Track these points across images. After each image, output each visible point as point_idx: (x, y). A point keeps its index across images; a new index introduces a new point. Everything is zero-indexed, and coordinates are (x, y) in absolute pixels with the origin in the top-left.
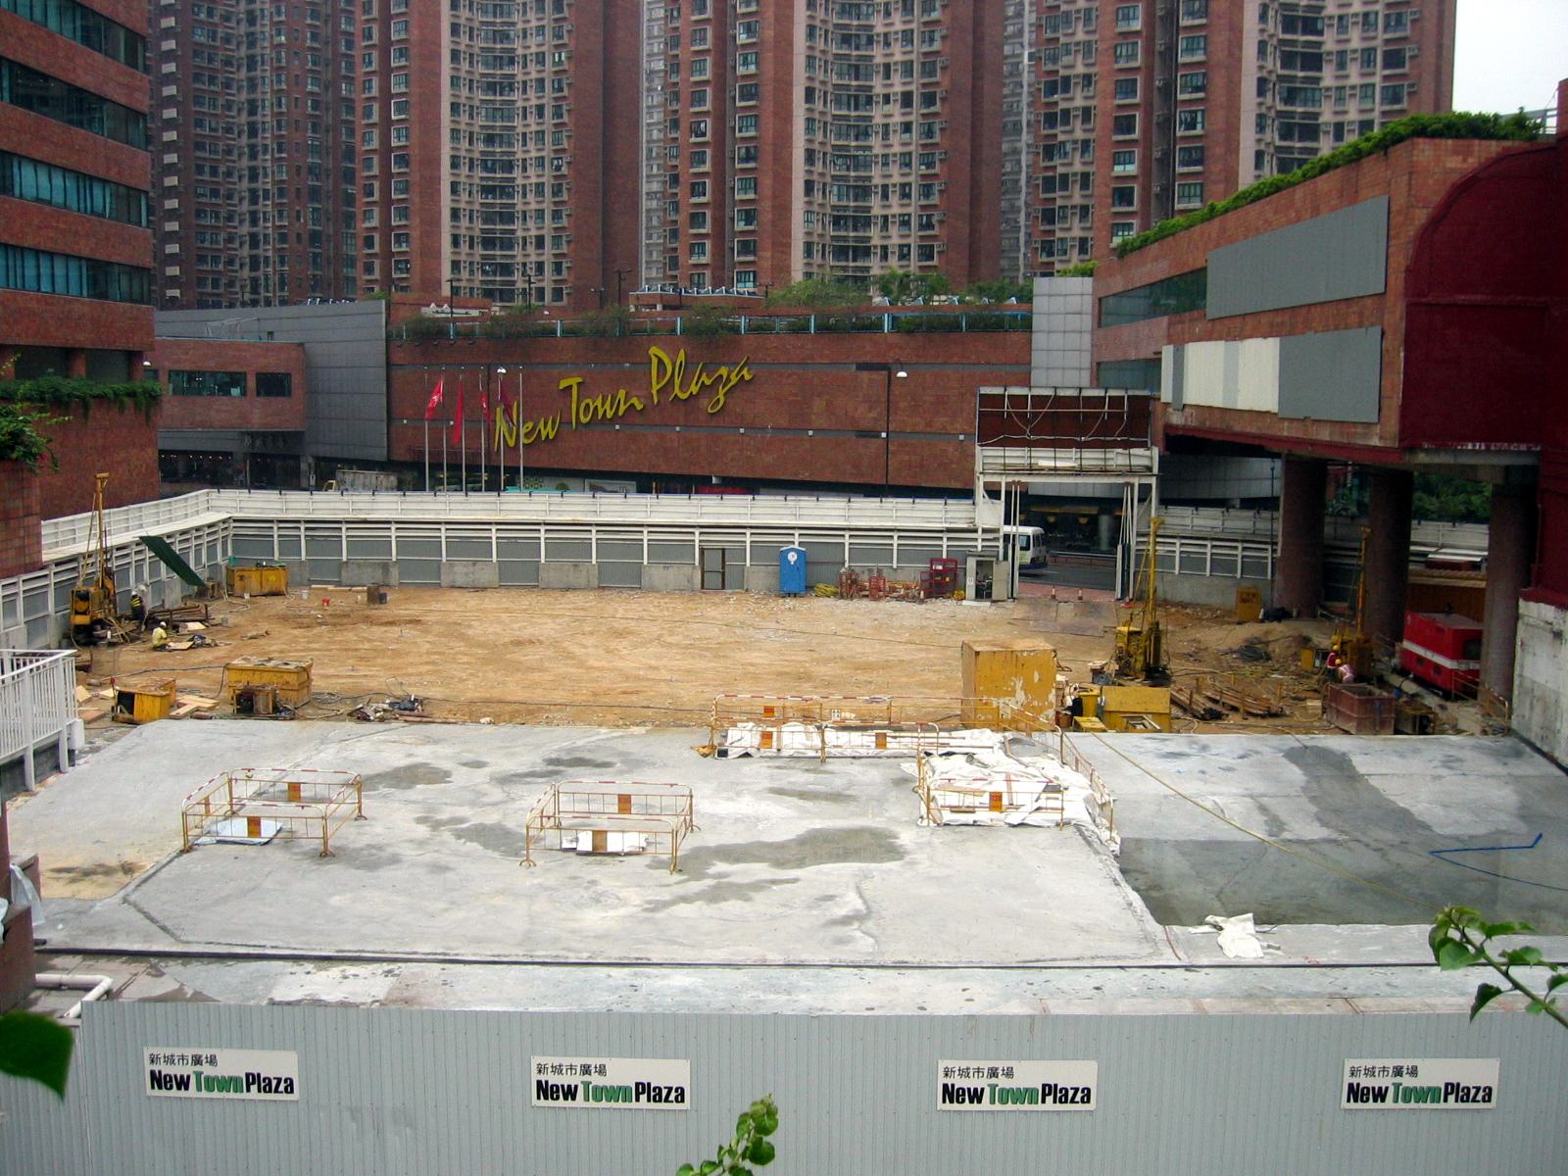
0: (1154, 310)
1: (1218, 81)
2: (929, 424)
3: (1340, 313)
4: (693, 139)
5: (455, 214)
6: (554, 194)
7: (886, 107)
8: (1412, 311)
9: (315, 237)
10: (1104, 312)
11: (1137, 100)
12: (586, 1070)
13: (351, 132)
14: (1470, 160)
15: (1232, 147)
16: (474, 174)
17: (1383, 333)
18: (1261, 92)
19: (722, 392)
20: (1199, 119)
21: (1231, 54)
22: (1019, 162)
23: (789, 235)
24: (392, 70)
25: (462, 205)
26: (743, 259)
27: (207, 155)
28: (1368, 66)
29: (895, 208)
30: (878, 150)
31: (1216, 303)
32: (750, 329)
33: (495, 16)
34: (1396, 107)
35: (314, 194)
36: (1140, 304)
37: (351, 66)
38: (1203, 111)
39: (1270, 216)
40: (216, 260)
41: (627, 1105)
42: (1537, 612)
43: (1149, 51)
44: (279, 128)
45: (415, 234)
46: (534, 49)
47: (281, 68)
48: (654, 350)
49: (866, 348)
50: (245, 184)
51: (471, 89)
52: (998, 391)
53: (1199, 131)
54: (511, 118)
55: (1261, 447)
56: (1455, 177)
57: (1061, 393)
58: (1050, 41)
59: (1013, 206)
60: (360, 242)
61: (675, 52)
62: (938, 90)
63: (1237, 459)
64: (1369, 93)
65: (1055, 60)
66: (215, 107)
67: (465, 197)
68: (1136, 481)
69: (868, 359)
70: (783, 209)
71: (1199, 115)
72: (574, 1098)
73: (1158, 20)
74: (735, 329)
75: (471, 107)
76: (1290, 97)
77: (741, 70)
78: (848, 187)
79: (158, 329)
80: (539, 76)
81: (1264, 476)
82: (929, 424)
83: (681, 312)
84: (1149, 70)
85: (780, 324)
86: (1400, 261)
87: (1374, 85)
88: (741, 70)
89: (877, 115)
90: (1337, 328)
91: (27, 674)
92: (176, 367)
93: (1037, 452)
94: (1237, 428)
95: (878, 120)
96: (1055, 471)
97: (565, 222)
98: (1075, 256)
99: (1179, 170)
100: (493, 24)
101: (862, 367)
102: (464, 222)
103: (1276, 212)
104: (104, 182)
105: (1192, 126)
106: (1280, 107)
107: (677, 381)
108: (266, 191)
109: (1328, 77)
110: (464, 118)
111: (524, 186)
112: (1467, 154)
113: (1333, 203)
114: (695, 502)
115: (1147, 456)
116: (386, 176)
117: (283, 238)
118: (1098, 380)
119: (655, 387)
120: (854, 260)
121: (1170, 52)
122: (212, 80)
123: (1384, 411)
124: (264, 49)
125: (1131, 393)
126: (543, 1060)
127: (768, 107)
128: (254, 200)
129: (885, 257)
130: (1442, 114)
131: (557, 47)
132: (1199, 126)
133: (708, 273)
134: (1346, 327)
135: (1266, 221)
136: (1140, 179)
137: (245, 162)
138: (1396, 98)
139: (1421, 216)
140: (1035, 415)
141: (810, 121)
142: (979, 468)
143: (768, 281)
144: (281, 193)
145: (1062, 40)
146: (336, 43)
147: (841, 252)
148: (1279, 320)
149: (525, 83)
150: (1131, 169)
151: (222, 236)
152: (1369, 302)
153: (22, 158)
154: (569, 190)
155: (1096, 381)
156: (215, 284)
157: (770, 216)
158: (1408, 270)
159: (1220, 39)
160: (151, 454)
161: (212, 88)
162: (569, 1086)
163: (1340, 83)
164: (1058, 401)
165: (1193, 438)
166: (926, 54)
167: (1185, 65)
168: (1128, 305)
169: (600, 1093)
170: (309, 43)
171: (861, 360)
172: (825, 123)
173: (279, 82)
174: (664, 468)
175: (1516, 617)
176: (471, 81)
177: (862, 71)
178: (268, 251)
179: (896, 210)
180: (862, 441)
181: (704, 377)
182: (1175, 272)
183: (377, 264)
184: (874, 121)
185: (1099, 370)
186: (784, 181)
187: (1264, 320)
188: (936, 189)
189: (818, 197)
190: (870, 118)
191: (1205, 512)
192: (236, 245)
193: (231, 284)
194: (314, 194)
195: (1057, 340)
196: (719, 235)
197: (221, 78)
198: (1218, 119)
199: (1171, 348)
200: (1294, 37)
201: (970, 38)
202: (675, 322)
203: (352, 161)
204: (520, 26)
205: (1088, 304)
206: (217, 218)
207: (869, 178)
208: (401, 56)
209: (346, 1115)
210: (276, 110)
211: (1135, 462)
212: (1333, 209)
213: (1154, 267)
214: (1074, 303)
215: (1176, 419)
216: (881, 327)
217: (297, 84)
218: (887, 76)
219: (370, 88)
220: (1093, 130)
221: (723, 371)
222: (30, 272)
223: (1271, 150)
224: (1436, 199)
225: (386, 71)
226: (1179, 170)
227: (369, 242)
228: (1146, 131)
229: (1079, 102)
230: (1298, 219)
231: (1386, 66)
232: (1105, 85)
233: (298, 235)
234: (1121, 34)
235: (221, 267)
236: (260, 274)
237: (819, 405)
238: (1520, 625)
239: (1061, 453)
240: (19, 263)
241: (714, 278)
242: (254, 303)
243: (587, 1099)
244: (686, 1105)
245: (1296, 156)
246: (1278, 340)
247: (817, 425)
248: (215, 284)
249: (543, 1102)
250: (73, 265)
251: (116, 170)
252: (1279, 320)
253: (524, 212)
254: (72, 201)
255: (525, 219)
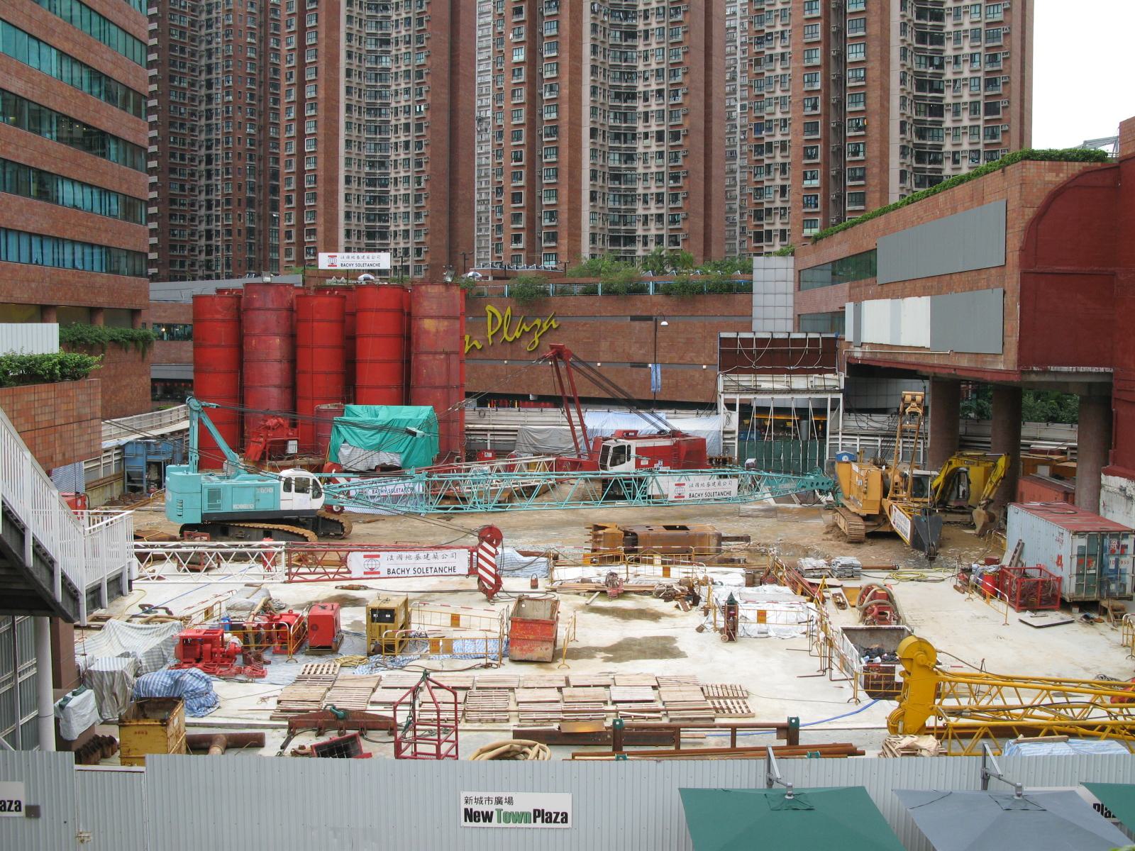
0: (835, 278)
1: (874, 123)
2: (681, 358)
3: (973, 279)
4: (514, 164)
5: (348, 215)
6: (416, 201)
7: (646, 141)
8: (1024, 276)
9: (250, 232)
10: (801, 282)
11: (818, 136)
12: (499, 801)
13: (277, 161)
14: (1061, 175)
15: (885, 168)
16: (361, 188)
17: (1004, 293)
18: (903, 131)
19: (536, 337)
20: (861, 149)
21: (882, 106)
22: (735, 178)
23: (580, 229)
24: (305, 118)
25: (353, 210)
26: (548, 245)
27: (178, 177)
28: (975, 113)
29: (653, 209)
30: (641, 170)
31: (886, 270)
32: (555, 293)
33: (376, 81)
34: (994, 141)
35: (250, 202)
36: (827, 274)
37: (277, 115)
38: (864, 144)
39: (921, 213)
40: (182, 248)
41: (528, 825)
42: (1113, 482)
43: (826, 103)
44: (227, 158)
45: (320, 229)
46: (403, 103)
47: (229, 117)
48: (489, 308)
49: (639, 305)
50: (203, 197)
51: (359, 131)
52: (733, 335)
53: (861, 157)
54: (386, 150)
55: (915, 371)
56: (1051, 187)
57: (776, 336)
58: (757, 96)
59: (731, 208)
60: (282, 235)
61: (499, 105)
62: (681, 130)
63: (894, 380)
64: (976, 132)
65: (761, 109)
66: (184, 144)
67: (354, 203)
68: (829, 396)
69: (639, 313)
70: (575, 211)
71: (861, 146)
72: (490, 821)
73: (831, 83)
74: (545, 292)
75: (360, 143)
76: (921, 134)
77: (546, 117)
78: (620, 195)
79: (152, 296)
80: (407, 139)
81: (914, 394)
82: (681, 358)
83: (508, 281)
84: (827, 115)
85: (577, 289)
86: (1016, 243)
87: (979, 126)
88: (546, 117)
89: (640, 146)
90: (971, 289)
91: (105, 527)
92: (159, 321)
93: (760, 378)
94: (901, 359)
95: (640, 150)
96: (774, 391)
97: (422, 221)
98: (777, 241)
99: (849, 183)
100: (375, 86)
101: (634, 318)
102: (354, 221)
103: (925, 212)
104: (117, 194)
105: (856, 153)
106: (916, 141)
107: (505, 329)
108: (218, 201)
109: (948, 120)
110: (355, 150)
111: (396, 196)
112: (1058, 172)
113: (966, 205)
114: (523, 413)
115: (836, 380)
116: (301, 189)
117: (229, 232)
118: (799, 326)
119: (490, 333)
120: (625, 245)
121: (841, 105)
122: (182, 126)
123: (1006, 346)
124: (218, 104)
125: (823, 336)
126: (469, 794)
127: (565, 142)
128: (209, 207)
129: (645, 244)
130: (1026, 148)
131: (418, 101)
132: (861, 154)
133: (523, 254)
134: (978, 289)
135: (918, 217)
136: (822, 190)
137: (203, 182)
138: (994, 136)
139: (1030, 213)
140: (759, 352)
141: (594, 151)
142: (721, 388)
143: (566, 260)
144: (228, 202)
145: (766, 96)
146: (266, 101)
147: (615, 240)
148: (929, 284)
149: (396, 126)
150: (816, 183)
151: (187, 232)
152: (993, 271)
153: (63, 178)
154: (426, 198)
155: (798, 327)
156: (182, 264)
157: (566, 216)
158: (1021, 250)
159: (874, 95)
160: (146, 381)
161: (182, 131)
162: (487, 813)
163: (957, 125)
164: (774, 341)
165: (868, 365)
166: (672, 105)
167: (851, 112)
168: (818, 275)
169: (509, 817)
170: (248, 101)
171: (634, 314)
172: (604, 152)
173: (228, 127)
174: (496, 390)
175: (1100, 486)
176: (360, 125)
177: (629, 117)
178: (218, 241)
179: (654, 211)
180: (635, 370)
181: (524, 326)
182: (854, 252)
183: (294, 249)
184: (638, 151)
185: (799, 320)
186: (575, 191)
187: (919, 284)
188: (680, 197)
189: (599, 203)
190: (635, 149)
191: (876, 417)
192: (197, 238)
193: (193, 264)
194: (250, 202)
195: (770, 299)
196: (531, 228)
197: (188, 125)
198: (874, 149)
199: (852, 304)
200: (924, 94)
201: (702, 94)
202: (504, 289)
203: (278, 180)
204: (394, 87)
205: (791, 274)
206: (184, 219)
207: (635, 189)
208: (312, 109)
209: (331, 833)
210: (225, 161)
211: (828, 383)
212: (966, 209)
213: (839, 248)
214: (781, 274)
215: (858, 353)
216: (647, 292)
217: (240, 128)
218: (646, 120)
219: (291, 130)
220: (788, 157)
221: (538, 322)
222: (68, 257)
223: (911, 170)
224: (1039, 202)
225: (301, 119)
226: (849, 183)
227: (288, 235)
228: (826, 205)
229: (779, 138)
230: (942, 215)
231: (986, 114)
232: (798, 126)
233: (239, 230)
234: (807, 92)
235: (186, 253)
236: (213, 257)
237: (604, 345)
238: (1102, 492)
239: (777, 378)
240: (61, 251)
241: (528, 258)
242: (209, 277)
243: (499, 821)
244: (568, 825)
245: (928, 174)
246: (929, 298)
247: (602, 360)
248: (182, 158)
249: (468, 824)
250: (96, 251)
251: (126, 186)
252: (929, 284)
253: (395, 232)
254: (97, 209)
255: (395, 218)
